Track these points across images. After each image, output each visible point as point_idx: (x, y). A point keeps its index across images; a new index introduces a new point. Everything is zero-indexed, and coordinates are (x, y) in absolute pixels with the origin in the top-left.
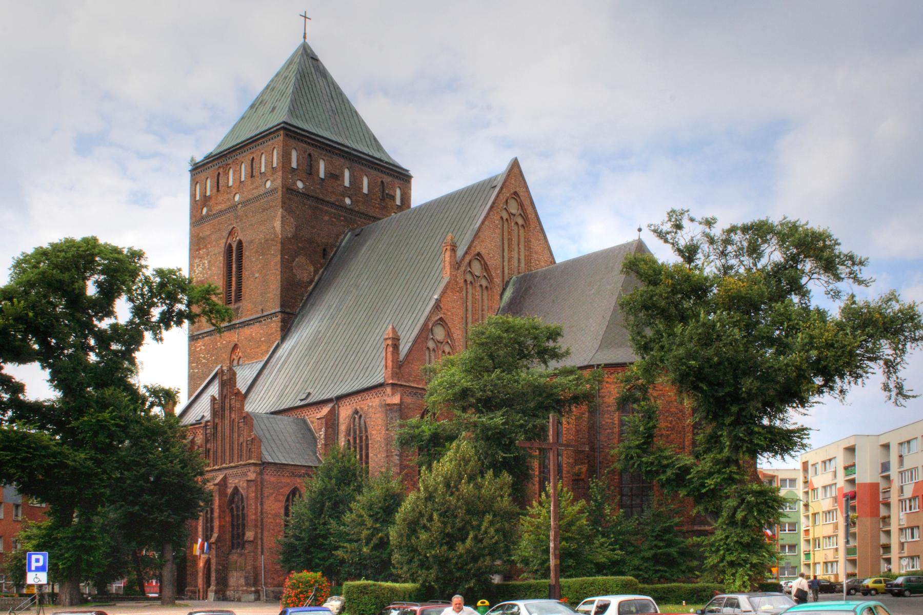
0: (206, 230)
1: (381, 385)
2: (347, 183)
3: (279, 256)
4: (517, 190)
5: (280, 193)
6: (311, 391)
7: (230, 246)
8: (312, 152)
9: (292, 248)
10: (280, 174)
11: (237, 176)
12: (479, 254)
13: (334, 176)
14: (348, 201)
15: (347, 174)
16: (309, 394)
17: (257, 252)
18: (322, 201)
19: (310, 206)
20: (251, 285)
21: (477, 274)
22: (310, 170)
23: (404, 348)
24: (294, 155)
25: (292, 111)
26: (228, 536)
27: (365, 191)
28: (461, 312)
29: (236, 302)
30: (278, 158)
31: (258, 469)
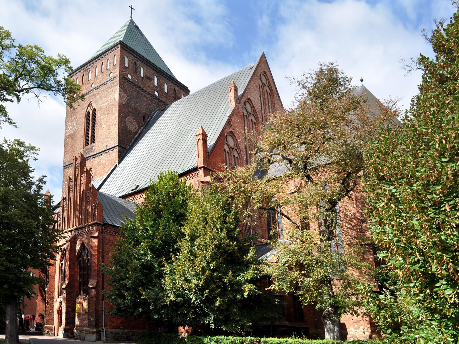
1: (195, 169)
2: (156, 84)
3: (118, 113)
4: (266, 71)
7: (89, 112)
8: (137, 62)
9: (124, 111)
10: (118, 68)
11: (94, 74)
14: (156, 94)
16: (138, 186)
17: (104, 113)
18: (142, 89)
19: (135, 90)
22: (136, 72)
23: (211, 142)
24: (126, 60)
25: (123, 39)
26: (77, 284)
27: (166, 91)
28: (259, 105)
29: (91, 143)
30: (117, 60)
31: (100, 228)
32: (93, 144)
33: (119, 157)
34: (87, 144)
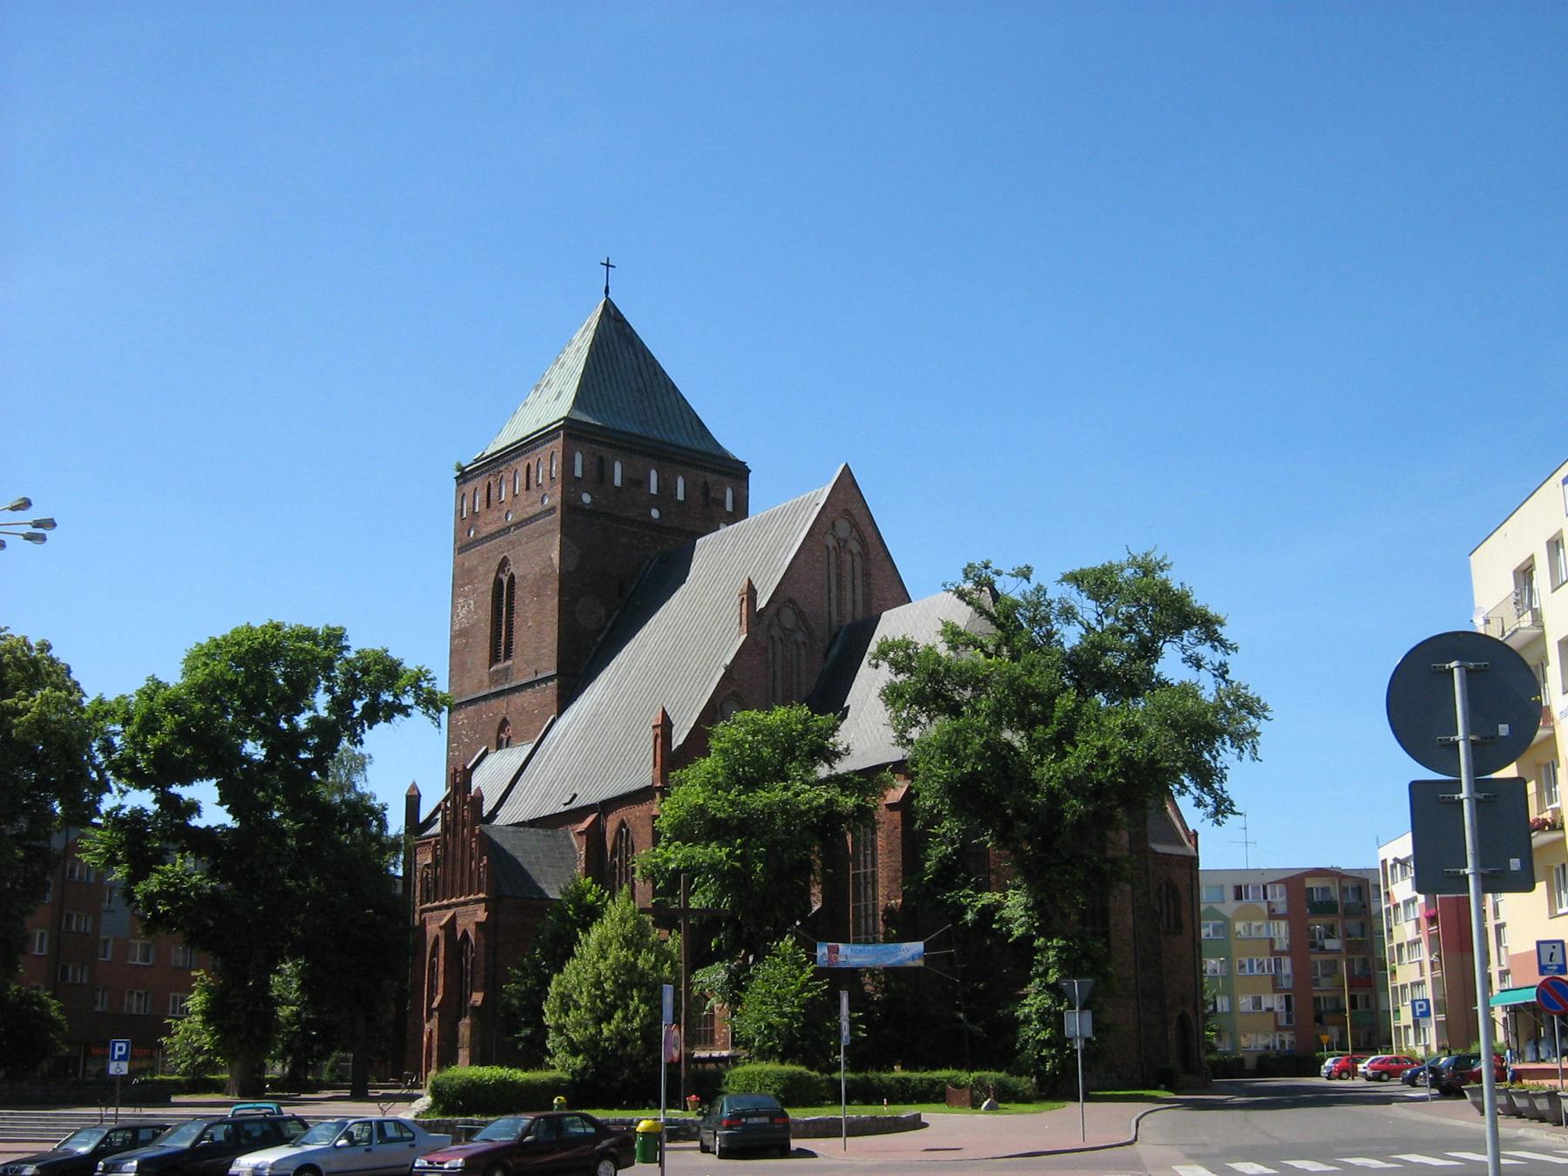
0: (472, 557)
2: (654, 490)
5: (558, 512)
6: (576, 791)
12: (791, 601)
13: (636, 482)
15: (654, 475)
20: (523, 637)
21: (788, 626)
22: (600, 473)
24: (578, 458)
27: (680, 497)
32: (509, 663)
33: (559, 699)
34: (494, 659)
